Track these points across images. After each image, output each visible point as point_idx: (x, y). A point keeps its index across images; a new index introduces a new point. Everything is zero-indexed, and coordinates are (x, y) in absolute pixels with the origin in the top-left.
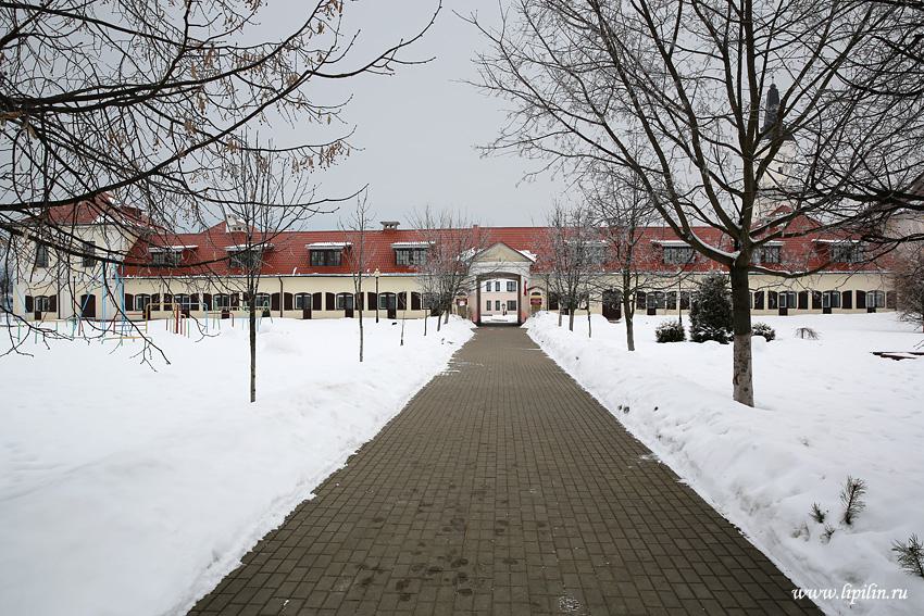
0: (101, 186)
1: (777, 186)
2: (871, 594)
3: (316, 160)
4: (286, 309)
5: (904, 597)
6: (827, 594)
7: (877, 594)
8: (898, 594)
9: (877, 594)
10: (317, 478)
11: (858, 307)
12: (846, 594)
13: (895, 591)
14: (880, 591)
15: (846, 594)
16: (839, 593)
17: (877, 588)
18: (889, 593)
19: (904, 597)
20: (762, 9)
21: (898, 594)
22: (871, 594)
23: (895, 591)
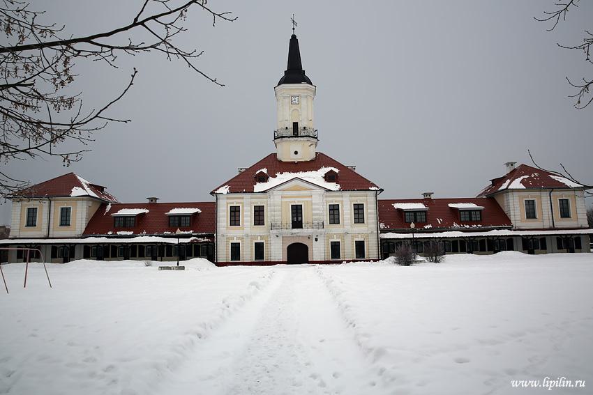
0: (556, 227)
1: (157, 47)
2: (562, 384)
3: (269, 280)
4: (339, 257)
5: (583, 386)
6: (534, 384)
7: (565, 384)
8: (579, 384)
9: (565, 384)
10: (303, 89)
11: (167, 256)
12: (546, 384)
13: (577, 382)
14: (567, 382)
15: (546, 384)
16: (541, 383)
17: (550, 380)
18: (573, 383)
19: (583, 386)
20: (3, 82)
21: (579, 384)
22: (562, 384)
23: (577, 382)
